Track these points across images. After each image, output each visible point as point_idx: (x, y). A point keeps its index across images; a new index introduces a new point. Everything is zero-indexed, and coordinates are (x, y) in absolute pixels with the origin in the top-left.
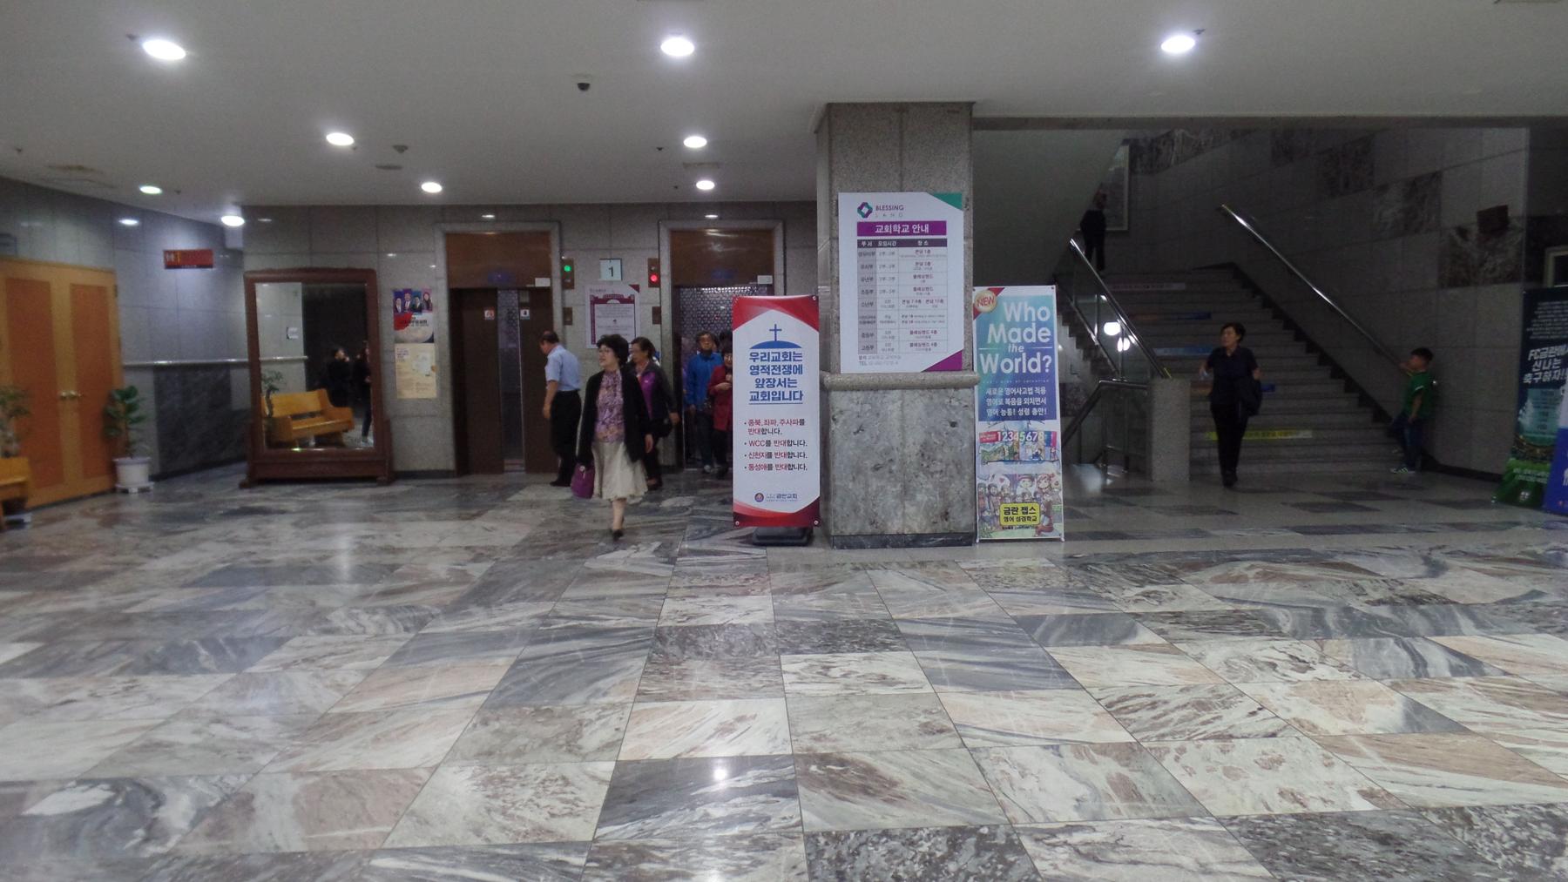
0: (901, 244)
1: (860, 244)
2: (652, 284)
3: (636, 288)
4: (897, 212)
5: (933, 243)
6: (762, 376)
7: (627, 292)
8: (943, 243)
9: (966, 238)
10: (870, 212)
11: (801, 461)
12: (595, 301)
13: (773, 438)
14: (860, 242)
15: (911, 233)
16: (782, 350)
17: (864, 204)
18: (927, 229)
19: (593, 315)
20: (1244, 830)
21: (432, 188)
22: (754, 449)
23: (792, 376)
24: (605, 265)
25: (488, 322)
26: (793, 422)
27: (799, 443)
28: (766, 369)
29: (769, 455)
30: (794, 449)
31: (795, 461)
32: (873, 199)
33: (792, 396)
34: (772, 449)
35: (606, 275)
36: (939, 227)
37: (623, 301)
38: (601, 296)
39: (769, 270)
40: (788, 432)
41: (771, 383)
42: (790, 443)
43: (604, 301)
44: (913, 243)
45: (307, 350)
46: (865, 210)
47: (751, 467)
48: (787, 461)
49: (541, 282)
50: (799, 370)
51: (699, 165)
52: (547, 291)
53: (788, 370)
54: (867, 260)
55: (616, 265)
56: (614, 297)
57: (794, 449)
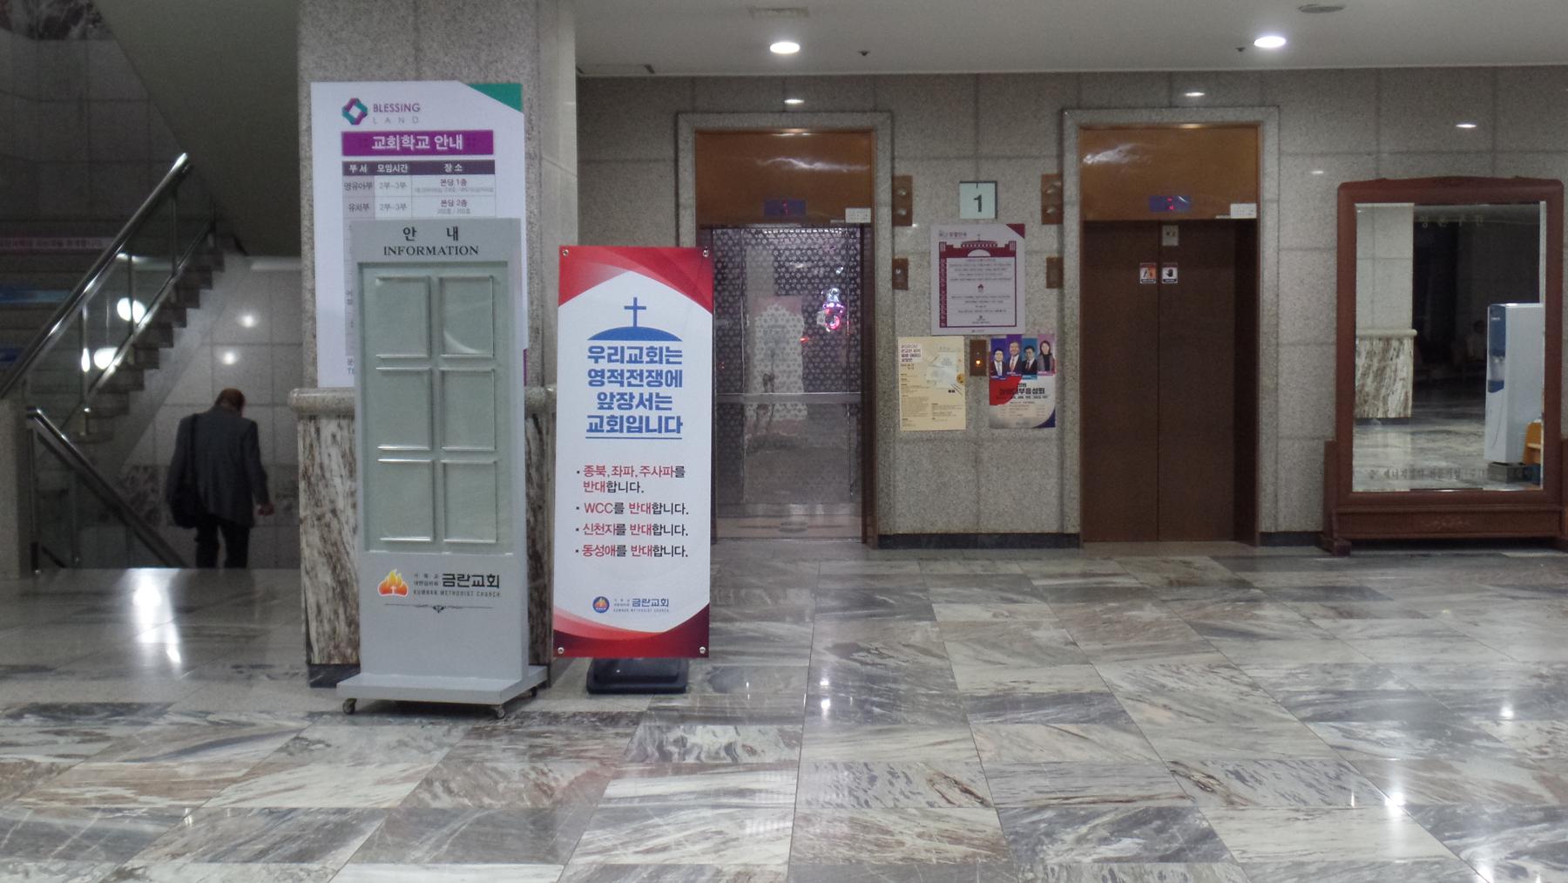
0: (416, 169)
1: (347, 170)
2: (1047, 219)
3: (1019, 229)
4: (408, 115)
5: (470, 168)
6: (611, 388)
7: (1003, 236)
8: (488, 168)
9: (310, 158)
10: (364, 114)
12: (948, 252)
14: (346, 166)
15: (433, 151)
16: (645, 344)
18: (460, 143)
21: (1270, 42)
22: (594, 518)
23: (664, 391)
24: (968, 192)
25: (1147, 286)
26: (665, 471)
28: (616, 376)
29: (620, 530)
30: (666, 519)
31: (666, 541)
33: (663, 425)
34: (626, 518)
35: (968, 210)
36: (480, 141)
37: (996, 252)
38: (957, 244)
39: (868, 201)
40: (656, 489)
41: (626, 402)
42: (657, 508)
43: (963, 252)
44: (437, 169)
45: (1354, 346)
46: (355, 112)
47: (588, 550)
48: (612, 540)
50: (676, 379)
53: (657, 379)
54: (359, 196)
55: (987, 191)
56: (980, 245)
57: (666, 519)
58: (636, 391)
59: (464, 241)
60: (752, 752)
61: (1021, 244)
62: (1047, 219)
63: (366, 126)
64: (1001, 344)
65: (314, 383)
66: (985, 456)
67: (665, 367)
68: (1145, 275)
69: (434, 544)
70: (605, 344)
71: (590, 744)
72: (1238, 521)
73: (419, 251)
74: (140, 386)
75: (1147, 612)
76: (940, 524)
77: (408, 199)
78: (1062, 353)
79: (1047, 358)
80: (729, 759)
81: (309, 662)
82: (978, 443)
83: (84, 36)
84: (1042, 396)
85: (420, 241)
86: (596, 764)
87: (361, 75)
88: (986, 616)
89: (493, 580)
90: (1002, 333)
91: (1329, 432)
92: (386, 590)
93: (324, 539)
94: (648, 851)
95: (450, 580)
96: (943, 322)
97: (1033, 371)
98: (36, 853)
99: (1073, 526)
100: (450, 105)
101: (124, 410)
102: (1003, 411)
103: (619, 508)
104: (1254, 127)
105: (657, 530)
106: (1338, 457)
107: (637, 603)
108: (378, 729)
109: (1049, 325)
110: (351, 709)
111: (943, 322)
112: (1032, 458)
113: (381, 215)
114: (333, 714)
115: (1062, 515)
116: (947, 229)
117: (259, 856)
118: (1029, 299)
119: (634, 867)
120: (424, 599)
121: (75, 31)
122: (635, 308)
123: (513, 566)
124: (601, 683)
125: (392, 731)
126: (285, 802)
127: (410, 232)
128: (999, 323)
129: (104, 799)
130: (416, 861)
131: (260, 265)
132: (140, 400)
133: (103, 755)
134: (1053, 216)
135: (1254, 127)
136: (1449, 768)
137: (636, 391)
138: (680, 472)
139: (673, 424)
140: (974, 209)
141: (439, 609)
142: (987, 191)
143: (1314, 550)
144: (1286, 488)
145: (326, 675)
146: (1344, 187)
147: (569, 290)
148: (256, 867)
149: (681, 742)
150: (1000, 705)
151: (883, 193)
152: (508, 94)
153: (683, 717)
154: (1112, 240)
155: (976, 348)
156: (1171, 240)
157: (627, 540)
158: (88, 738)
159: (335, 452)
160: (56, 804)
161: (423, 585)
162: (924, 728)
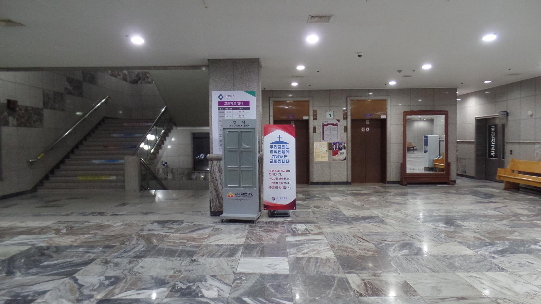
0: (233, 109)
1: (219, 109)
2: (344, 119)
3: (338, 121)
4: (232, 98)
5: (245, 109)
6: (274, 154)
7: (335, 122)
8: (248, 108)
11: (289, 185)
12: (324, 125)
13: (278, 177)
14: (219, 108)
15: (237, 105)
17: (221, 95)
19: (323, 130)
20: (193, 293)
21: (392, 83)
22: (271, 181)
23: (286, 154)
24: (328, 113)
26: (286, 171)
27: (288, 179)
28: (276, 151)
30: (286, 181)
31: (286, 185)
32: (224, 93)
33: (286, 161)
34: (278, 181)
35: (328, 117)
36: (247, 103)
37: (334, 125)
39: (308, 115)
40: (284, 175)
42: (284, 179)
43: (327, 125)
44: (238, 109)
46: (221, 97)
47: (270, 187)
48: (275, 185)
49: (305, 118)
50: (288, 152)
51: (298, 76)
52: (307, 122)
53: (284, 152)
54: (222, 115)
55: (332, 113)
57: (286, 181)
58: (280, 154)
59: (246, 123)
60: (312, 230)
61: (339, 124)
62: (344, 119)
63: (223, 100)
64: (335, 144)
65: (212, 153)
66: (332, 166)
67: (286, 149)
68: (363, 130)
69: (240, 187)
70: (273, 145)
71: (277, 229)
72: (382, 178)
73: (236, 126)
74: (158, 153)
75: (374, 199)
76: (322, 180)
77: (232, 115)
78: (347, 146)
79: (344, 146)
80: (307, 232)
81: (211, 211)
82: (330, 163)
83: (141, 83)
84: (343, 154)
85: (236, 124)
86: (280, 234)
87: (222, 90)
88: (341, 199)
89: (252, 194)
90: (335, 141)
91: (401, 161)
92: (229, 196)
93: (214, 186)
94: (303, 254)
95: (242, 194)
96: (323, 139)
97: (341, 149)
98: (172, 256)
99: (350, 181)
100: (240, 96)
101: (156, 158)
102: (335, 157)
103: (277, 179)
104: (385, 100)
105: (285, 183)
106: (403, 166)
107: (281, 198)
108: (230, 226)
109: (345, 140)
110: (223, 221)
111: (323, 139)
112: (341, 167)
113: (226, 118)
114: (219, 222)
115: (347, 178)
116: (324, 121)
117: (221, 256)
118: (341, 134)
119: (303, 258)
120: (237, 198)
121: (139, 82)
122: (280, 137)
123: (256, 191)
124: (272, 215)
125: (233, 226)
126: (220, 243)
127: (234, 122)
128: (334, 139)
129: (180, 242)
130: (255, 257)
131: (179, 128)
132: (158, 155)
133: (175, 232)
134: (345, 118)
135: (385, 100)
136: (461, 233)
137: (280, 154)
138: (289, 171)
139: (288, 161)
140: (329, 117)
141: (240, 200)
142: (332, 113)
143: (398, 185)
144: (392, 173)
145: (216, 213)
146: (404, 112)
147: (265, 134)
148: (221, 258)
149: (295, 228)
150: (356, 219)
151: (311, 113)
152: (252, 93)
153: (292, 222)
154: (357, 123)
155: (330, 144)
156: (368, 123)
157: (278, 185)
158: (170, 228)
159: (216, 167)
160: (171, 244)
161: (237, 195)
162: (344, 225)
